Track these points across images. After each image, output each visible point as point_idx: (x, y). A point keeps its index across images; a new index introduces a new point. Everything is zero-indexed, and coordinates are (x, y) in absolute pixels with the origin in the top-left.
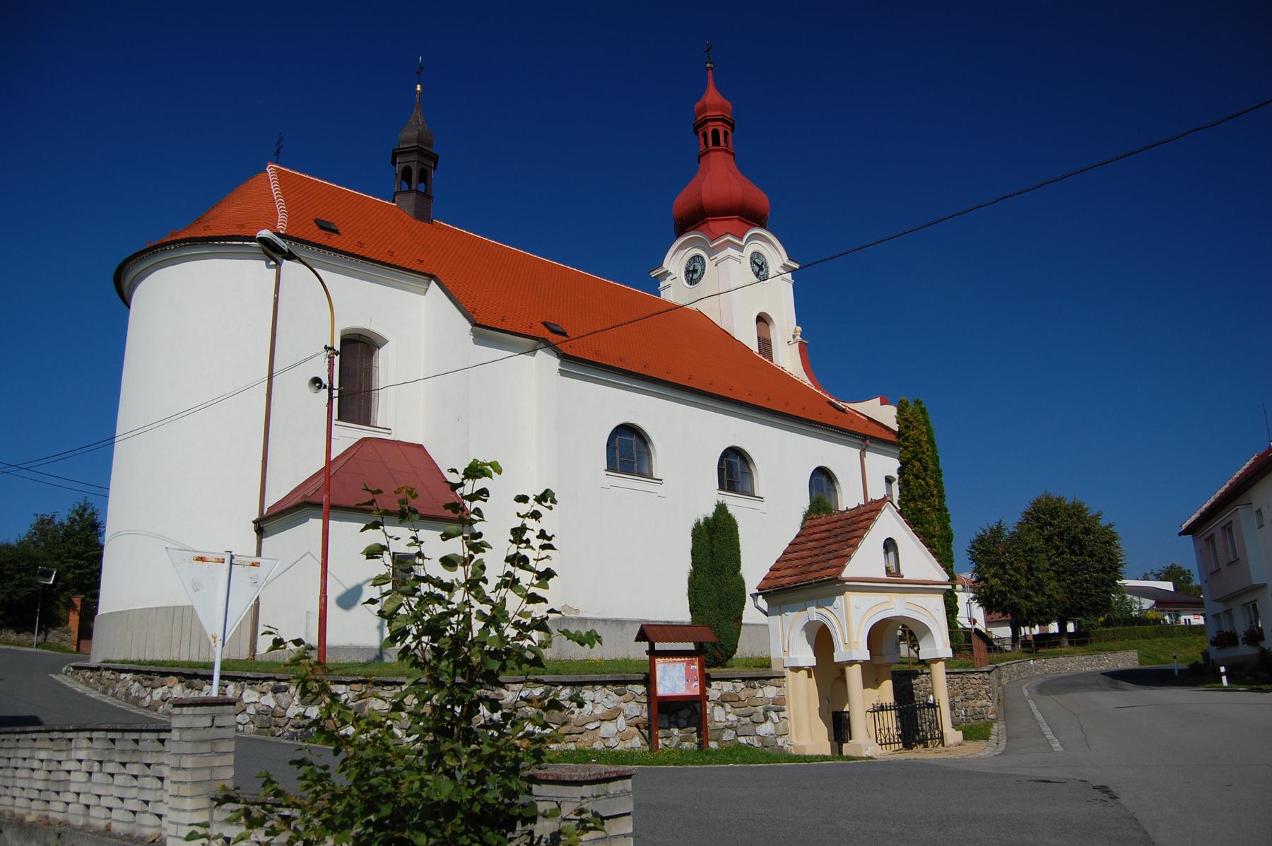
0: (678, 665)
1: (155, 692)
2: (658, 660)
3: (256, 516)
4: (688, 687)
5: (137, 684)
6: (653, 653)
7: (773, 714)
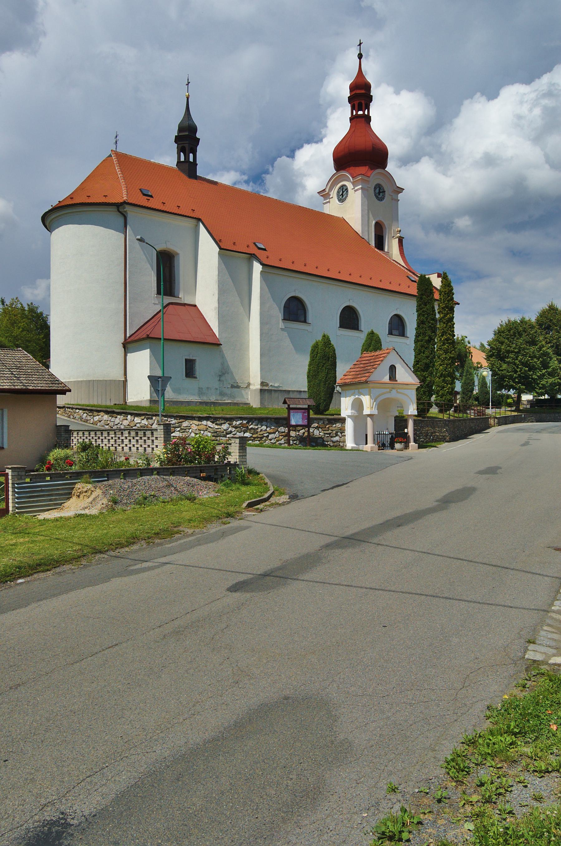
0: (299, 413)
1: (95, 418)
2: (291, 411)
3: (122, 340)
4: (303, 422)
5: (85, 415)
6: (289, 409)
7: (339, 433)
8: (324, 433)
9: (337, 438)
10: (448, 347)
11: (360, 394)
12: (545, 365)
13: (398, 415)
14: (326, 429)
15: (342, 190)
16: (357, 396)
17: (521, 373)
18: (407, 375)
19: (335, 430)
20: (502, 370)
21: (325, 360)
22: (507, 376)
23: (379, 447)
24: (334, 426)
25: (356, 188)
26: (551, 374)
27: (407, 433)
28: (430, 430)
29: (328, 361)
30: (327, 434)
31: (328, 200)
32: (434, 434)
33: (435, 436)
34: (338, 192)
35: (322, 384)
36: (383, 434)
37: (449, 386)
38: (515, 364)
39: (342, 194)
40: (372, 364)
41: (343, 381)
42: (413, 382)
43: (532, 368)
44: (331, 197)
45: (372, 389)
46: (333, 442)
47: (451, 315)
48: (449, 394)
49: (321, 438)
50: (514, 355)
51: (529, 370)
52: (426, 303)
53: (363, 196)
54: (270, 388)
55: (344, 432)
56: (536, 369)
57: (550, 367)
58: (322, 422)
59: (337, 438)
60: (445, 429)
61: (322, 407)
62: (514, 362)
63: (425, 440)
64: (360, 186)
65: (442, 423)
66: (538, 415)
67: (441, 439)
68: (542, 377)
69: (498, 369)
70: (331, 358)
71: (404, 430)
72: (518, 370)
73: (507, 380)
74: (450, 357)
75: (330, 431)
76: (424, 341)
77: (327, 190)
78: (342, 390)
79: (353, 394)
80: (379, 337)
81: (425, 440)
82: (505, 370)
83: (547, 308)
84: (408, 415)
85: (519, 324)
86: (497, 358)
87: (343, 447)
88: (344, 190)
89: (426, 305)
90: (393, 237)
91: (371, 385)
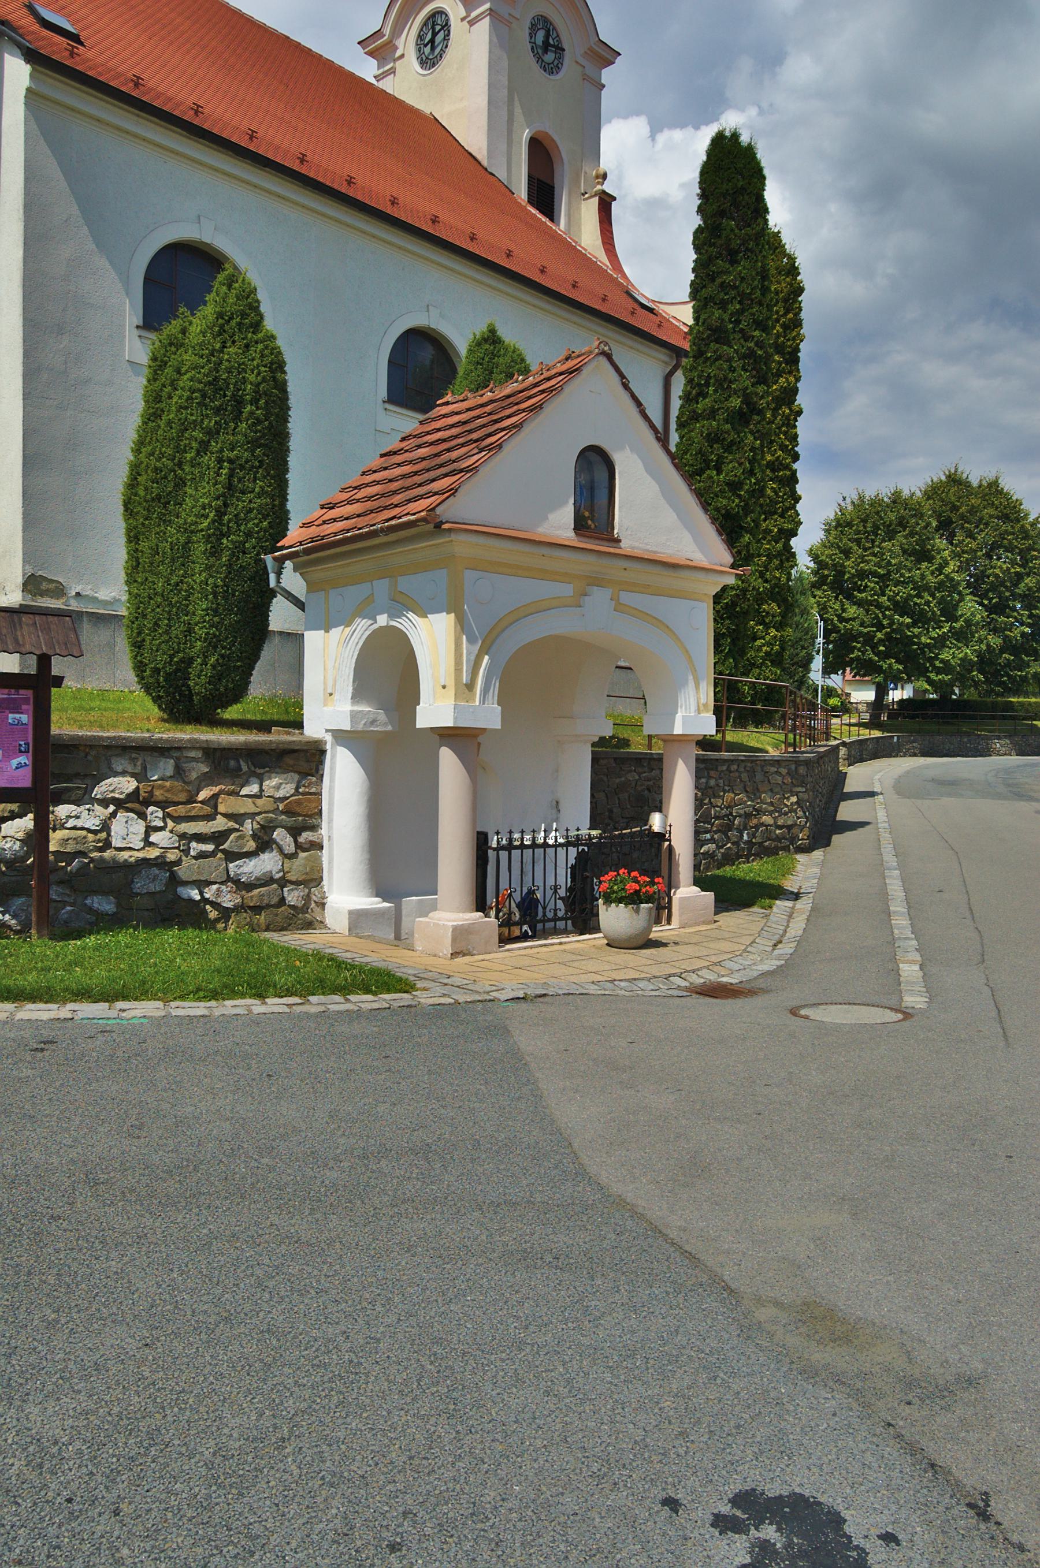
8: (182, 836)
9: (267, 863)
10: (776, 494)
11: (401, 604)
12: (950, 612)
13: (608, 732)
14: (196, 808)
15: (433, 28)
16: (382, 620)
17: (893, 631)
18: (670, 517)
19: (253, 816)
20: (847, 620)
21: (218, 411)
22: (861, 634)
23: (506, 923)
24: (253, 789)
25: (474, 14)
26: (962, 636)
27: (661, 837)
28: (741, 802)
29: (237, 418)
30: (199, 838)
31: (391, 65)
32: (755, 821)
33: (757, 827)
34: (420, 37)
35: (199, 548)
36: (534, 845)
37: (773, 632)
38: (879, 606)
39: (432, 41)
40: (475, 436)
41: (313, 531)
42: (699, 558)
43: (921, 619)
44: (398, 54)
45: (469, 575)
46: (240, 885)
47: (792, 379)
48: (772, 662)
49: (160, 863)
50: (877, 583)
51: (914, 624)
52: (737, 252)
53: (495, 39)
54: (74, 605)
55: (314, 828)
56: (928, 621)
57: (961, 616)
58: (168, 766)
59: (267, 863)
60: (794, 799)
61: (199, 681)
62: (876, 600)
63: (719, 847)
64: (487, 6)
65: (784, 771)
66: (928, 738)
67: (778, 839)
68: (941, 642)
69: (838, 616)
70: (255, 401)
71: (646, 821)
72: (885, 622)
73: (859, 645)
74: (781, 531)
75: (220, 824)
76: (721, 416)
77: (387, 31)
78: (312, 587)
79: (366, 609)
80: (523, 360)
81: (719, 847)
82: (853, 619)
83: (943, 478)
84: (671, 740)
85: (887, 506)
86: (832, 589)
87: (305, 909)
88: (438, 28)
89: (734, 262)
90: (583, 195)
91: (462, 546)
